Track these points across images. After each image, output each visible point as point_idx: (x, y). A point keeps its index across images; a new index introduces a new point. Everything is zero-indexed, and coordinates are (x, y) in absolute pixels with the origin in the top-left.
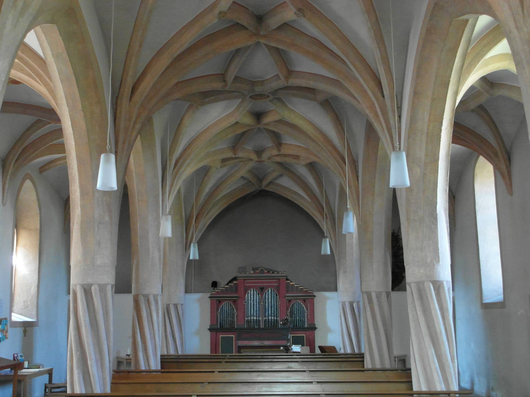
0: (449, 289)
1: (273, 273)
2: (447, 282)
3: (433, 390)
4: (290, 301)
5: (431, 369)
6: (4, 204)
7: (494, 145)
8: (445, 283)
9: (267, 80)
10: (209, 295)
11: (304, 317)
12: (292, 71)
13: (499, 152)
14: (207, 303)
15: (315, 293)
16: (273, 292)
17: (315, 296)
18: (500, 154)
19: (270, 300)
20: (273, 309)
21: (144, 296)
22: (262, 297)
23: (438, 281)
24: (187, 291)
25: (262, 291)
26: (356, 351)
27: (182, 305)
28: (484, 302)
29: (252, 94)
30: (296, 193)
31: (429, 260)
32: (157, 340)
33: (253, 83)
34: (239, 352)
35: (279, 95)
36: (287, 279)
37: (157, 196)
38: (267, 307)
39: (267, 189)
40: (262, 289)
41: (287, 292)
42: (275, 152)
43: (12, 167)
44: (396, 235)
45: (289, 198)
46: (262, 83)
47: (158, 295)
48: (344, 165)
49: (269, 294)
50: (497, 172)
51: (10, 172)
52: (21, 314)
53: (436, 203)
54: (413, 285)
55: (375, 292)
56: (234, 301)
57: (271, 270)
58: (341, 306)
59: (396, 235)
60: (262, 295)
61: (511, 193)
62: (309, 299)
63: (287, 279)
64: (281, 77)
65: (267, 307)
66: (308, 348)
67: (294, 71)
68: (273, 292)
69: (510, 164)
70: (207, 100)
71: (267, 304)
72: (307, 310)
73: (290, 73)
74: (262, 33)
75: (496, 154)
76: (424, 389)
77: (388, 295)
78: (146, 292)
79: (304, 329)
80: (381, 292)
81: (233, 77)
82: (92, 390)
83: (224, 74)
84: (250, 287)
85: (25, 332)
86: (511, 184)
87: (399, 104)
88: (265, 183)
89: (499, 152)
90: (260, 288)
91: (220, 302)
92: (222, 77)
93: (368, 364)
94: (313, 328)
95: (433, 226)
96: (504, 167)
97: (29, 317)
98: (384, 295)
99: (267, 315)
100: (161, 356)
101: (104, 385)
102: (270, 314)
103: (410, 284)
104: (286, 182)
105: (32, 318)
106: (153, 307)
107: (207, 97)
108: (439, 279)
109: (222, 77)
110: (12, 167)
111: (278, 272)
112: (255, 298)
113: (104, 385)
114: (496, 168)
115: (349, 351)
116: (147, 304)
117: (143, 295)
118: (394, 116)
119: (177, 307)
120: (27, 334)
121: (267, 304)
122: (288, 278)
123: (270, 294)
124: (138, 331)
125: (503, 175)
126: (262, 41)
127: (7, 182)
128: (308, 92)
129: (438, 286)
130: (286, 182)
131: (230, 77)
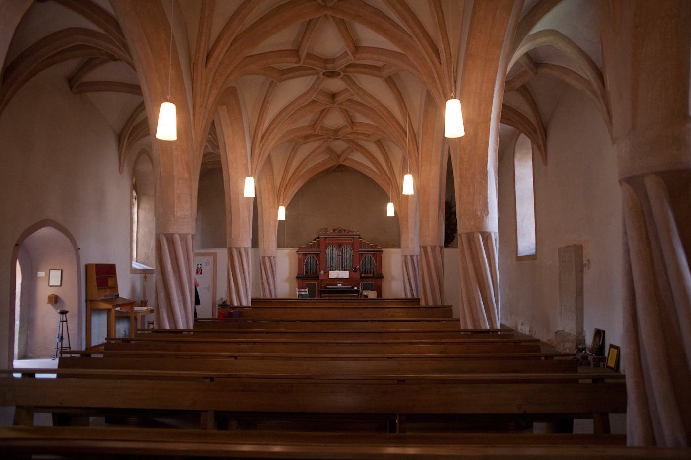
0: (495, 240)
1: (349, 233)
2: (494, 233)
3: (478, 328)
4: (362, 254)
5: (477, 310)
6: (121, 171)
7: (533, 122)
8: (492, 234)
9: (338, 57)
10: (296, 250)
11: (374, 269)
12: (358, 47)
13: (538, 128)
14: (295, 258)
15: (384, 249)
16: (348, 248)
17: (382, 251)
18: (538, 131)
19: (346, 254)
20: (348, 261)
21: (236, 248)
22: (339, 252)
23: (486, 232)
24: (280, 246)
25: (340, 247)
26: (415, 297)
27: (274, 257)
28: (519, 255)
29: (324, 71)
30: (367, 167)
31: (479, 213)
32: (248, 284)
33: (326, 61)
34: (320, 294)
35: (347, 72)
36: (360, 238)
37: (247, 164)
38: (343, 259)
39: (344, 164)
40: (340, 245)
41: (360, 247)
42: (349, 130)
43: (126, 141)
44: (449, 203)
45: (362, 171)
46: (333, 60)
47: (248, 248)
48: (406, 138)
49: (345, 249)
50: (534, 146)
51: (125, 144)
52: (143, 264)
53: (487, 161)
54: (463, 236)
55: (431, 246)
56: (317, 255)
57: (346, 230)
58: (403, 259)
59: (449, 203)
60: (339, 250)
61: (546, 163)
62: (377, 255)
63: (360, 238)
64: (349, 53)
65: (343, 259)
66: (375, 292)
67: (362, 47)
68: (348, 248)
69: (546, 139)
70: (284, 77)
71: (343, 258)
72: (376, 262)
73: (357, 48)
74: (328, 6)
75: (535, 132)
76: (470, 327)
77: (441, 247)
78: (238, 246)
79: (374, 277)
80: (435, 246)
81: (305, 53)
82: (176, 327)
83: (297, 50)
84: (329, 244)
85: (145, 277)
86: (546, 158)
87: (440, 264)
88: (341, 158)
89: (538, 128)
90: (338, 245)
91: (305, 256)
92: (296, 52)
93: (629, 444)
94: (380, 277)
95: (484, 182)
96: (541, 142)
97: (150, 266)
98: (438, 248)
99: (343, 266)
100: (252, 299)
101: (187, 323)
102: (346, 266)
103: (460, 235)
104: (358, 157)
105: (152, 267)
106: (244, 258)
107: (286, 74)
108: (486, 231)
109: (296, 52)
110: (126, 141)
111: (352, 232)
112: (334, 253)
113: (187, 323)
114: (533, 142)
115: (409, 296)
116: (239, 256)
117: (236, 248)
118: (450, 81)
119: (270, 259)
120: (147, 279)
121: (343, 258)
122: (361, 237)
123: (346, 249)
124: (232, 277)
125: (539, 148)
126: (329, 13)
127: (123, 153)
128: (374, 70)
129: (487, 237)
130: (358, 157)
131: (303, 55)
